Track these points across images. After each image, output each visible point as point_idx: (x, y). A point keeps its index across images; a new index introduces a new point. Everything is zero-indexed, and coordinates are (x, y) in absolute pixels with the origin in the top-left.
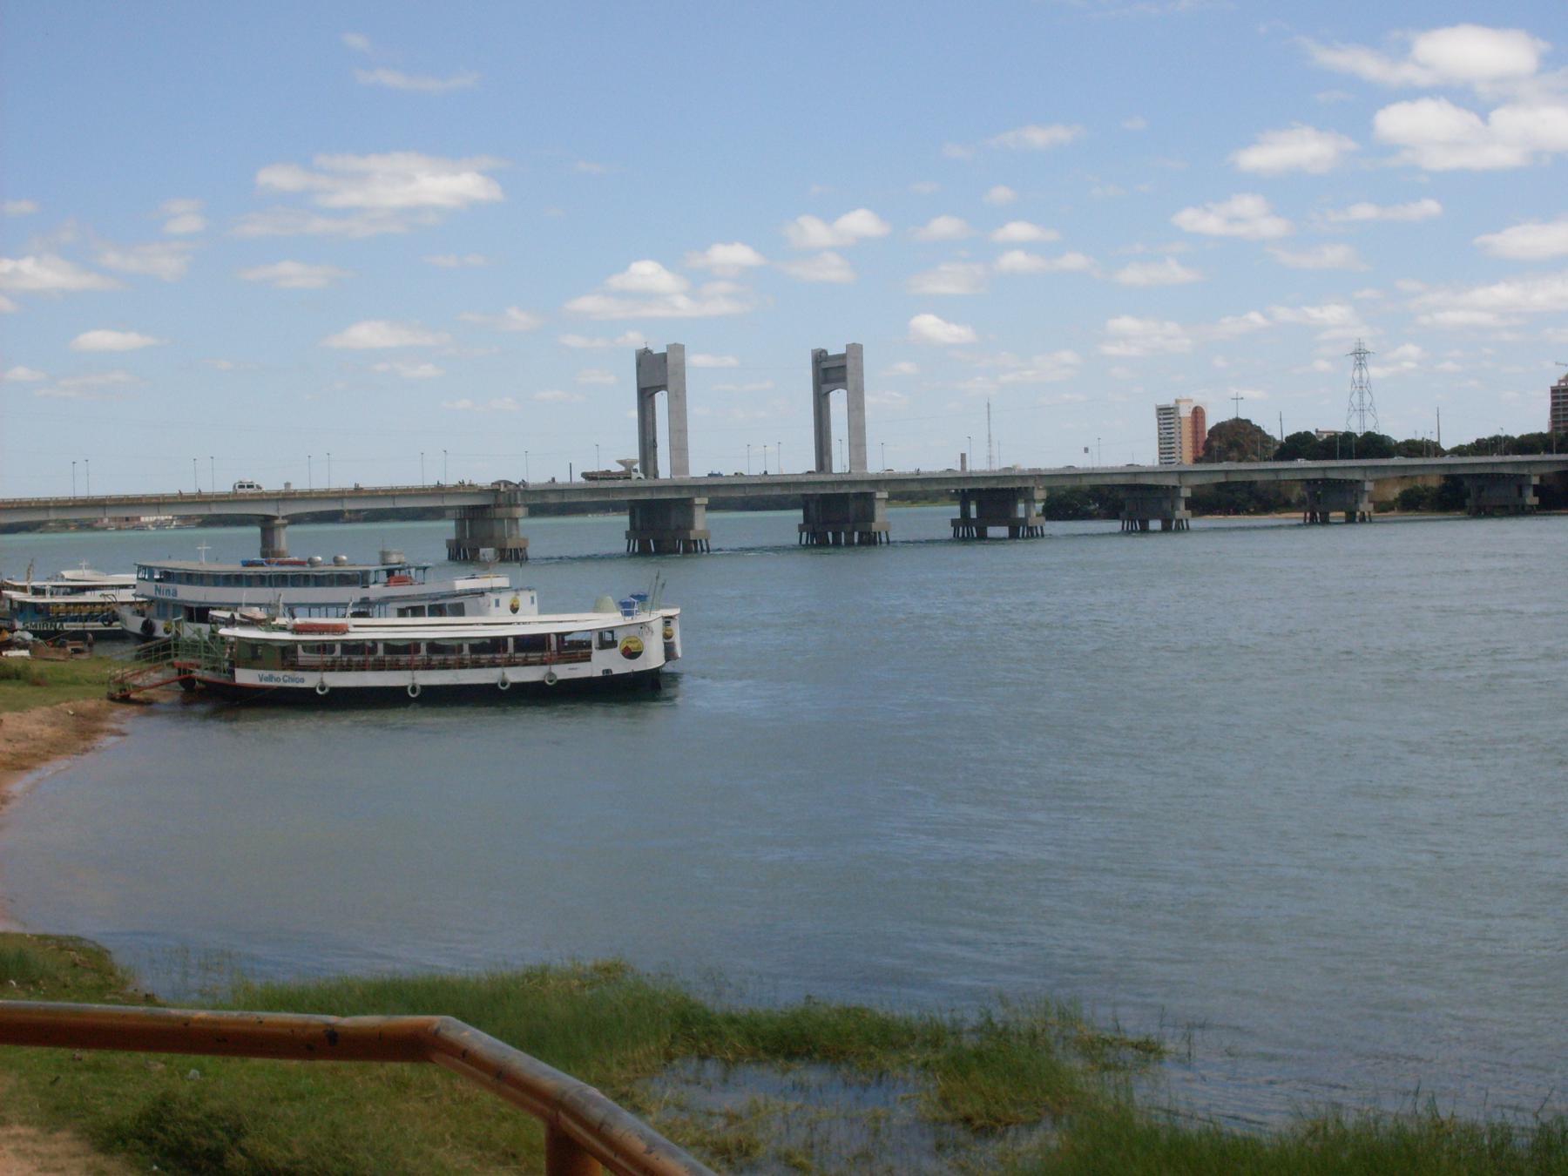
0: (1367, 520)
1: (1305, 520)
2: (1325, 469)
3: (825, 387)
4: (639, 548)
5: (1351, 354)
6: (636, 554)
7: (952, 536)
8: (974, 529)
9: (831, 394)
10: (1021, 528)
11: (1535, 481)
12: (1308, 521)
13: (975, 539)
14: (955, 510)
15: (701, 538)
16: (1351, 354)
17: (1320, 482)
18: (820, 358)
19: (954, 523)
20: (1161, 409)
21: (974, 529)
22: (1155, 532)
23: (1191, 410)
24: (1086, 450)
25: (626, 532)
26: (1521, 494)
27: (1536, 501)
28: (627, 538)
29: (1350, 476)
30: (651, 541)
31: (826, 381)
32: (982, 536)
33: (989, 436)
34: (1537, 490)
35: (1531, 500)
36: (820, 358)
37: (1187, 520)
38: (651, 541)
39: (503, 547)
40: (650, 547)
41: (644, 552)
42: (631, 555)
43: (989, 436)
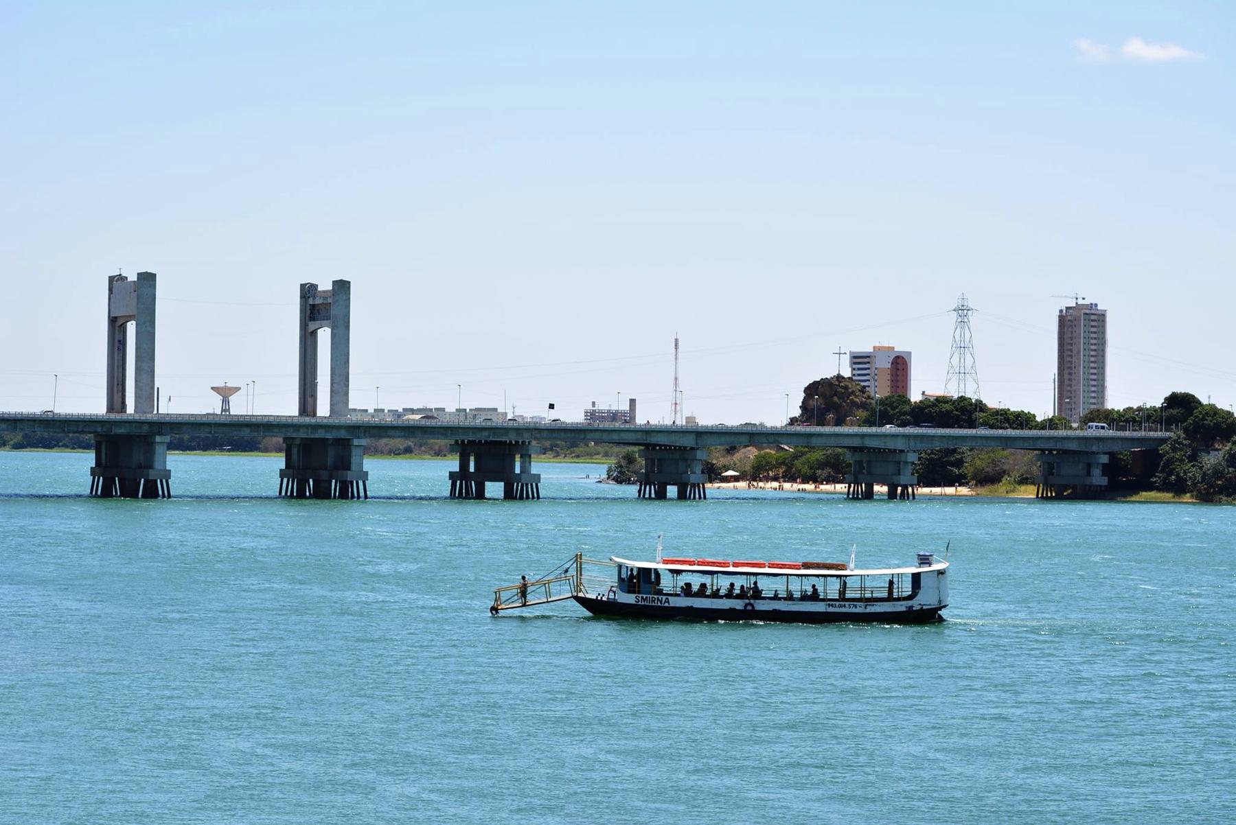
0: (911, 497)
1: (848, 496)
2: (863, 436)
3: (312, 326)
4: (101, 492)
5: (954, 310)
6: (288, 497)
7: (449, 495)
8: (473, 482)
9: (319, 331)
10: (515, 484)
11: (1104, 459)
12: (851, 496)
13: (653, 499)
14: (454, 465)
15: (699, 482)
16: (954, 310)
17: (1047, 452)
18: (308, 291)
19: (452, 476)
20: (855, 357)
21: (473, 482)
22: (671, 499)
23: (891, 360)
24: (552, 406)
25: (281, 470)
26: (1089, 474)
27: (1104, 481)
28: (91, 475)
29: (891, 445)
30: (117, 478)
31: (312, 319)
32: (480, 495)
33: (676, 379)
34: (1107, 470)
35: (1098, 479)
36: (308, 291)
37: (703, 485)
38: (117, 478)
39: (345, 479)
40: (144, 485)
41: (107, 493)
42: (93, 496)
43: (676, 379)
